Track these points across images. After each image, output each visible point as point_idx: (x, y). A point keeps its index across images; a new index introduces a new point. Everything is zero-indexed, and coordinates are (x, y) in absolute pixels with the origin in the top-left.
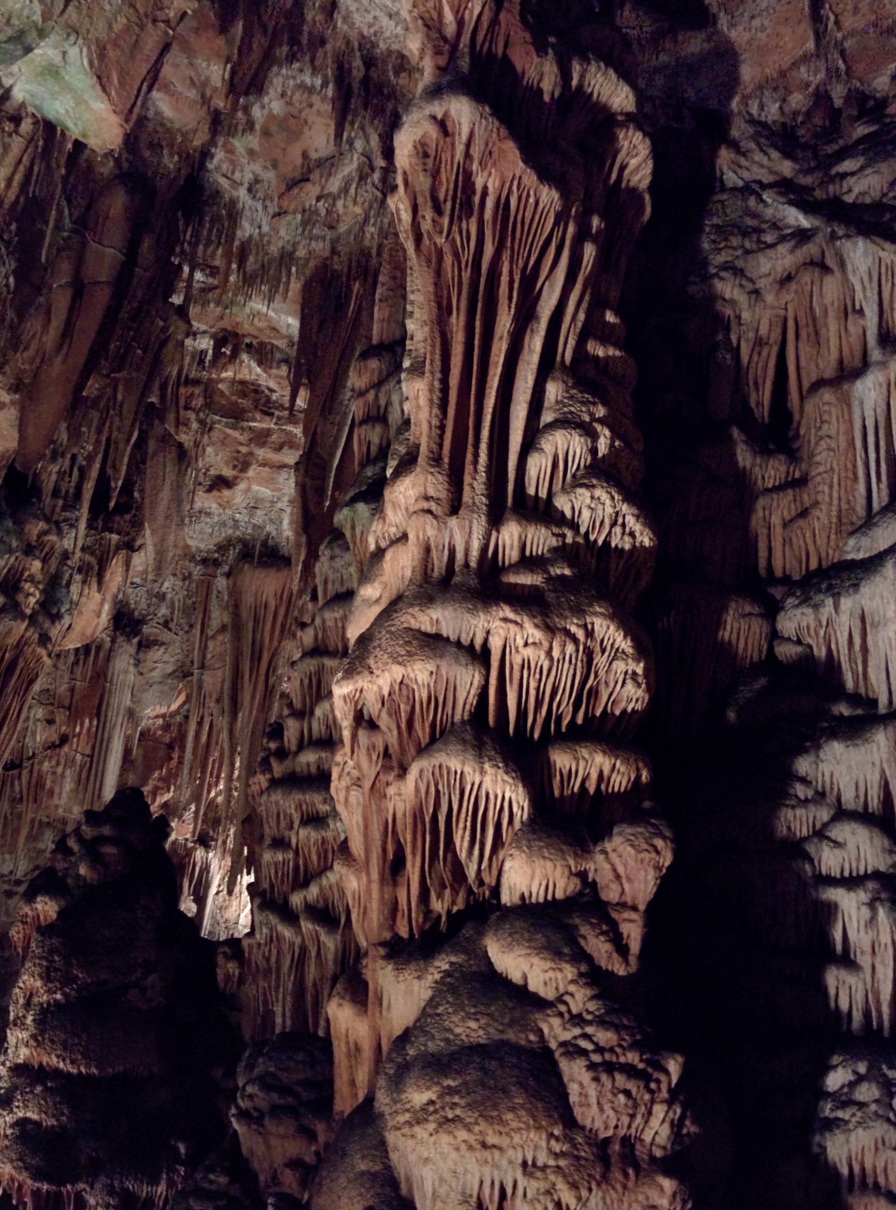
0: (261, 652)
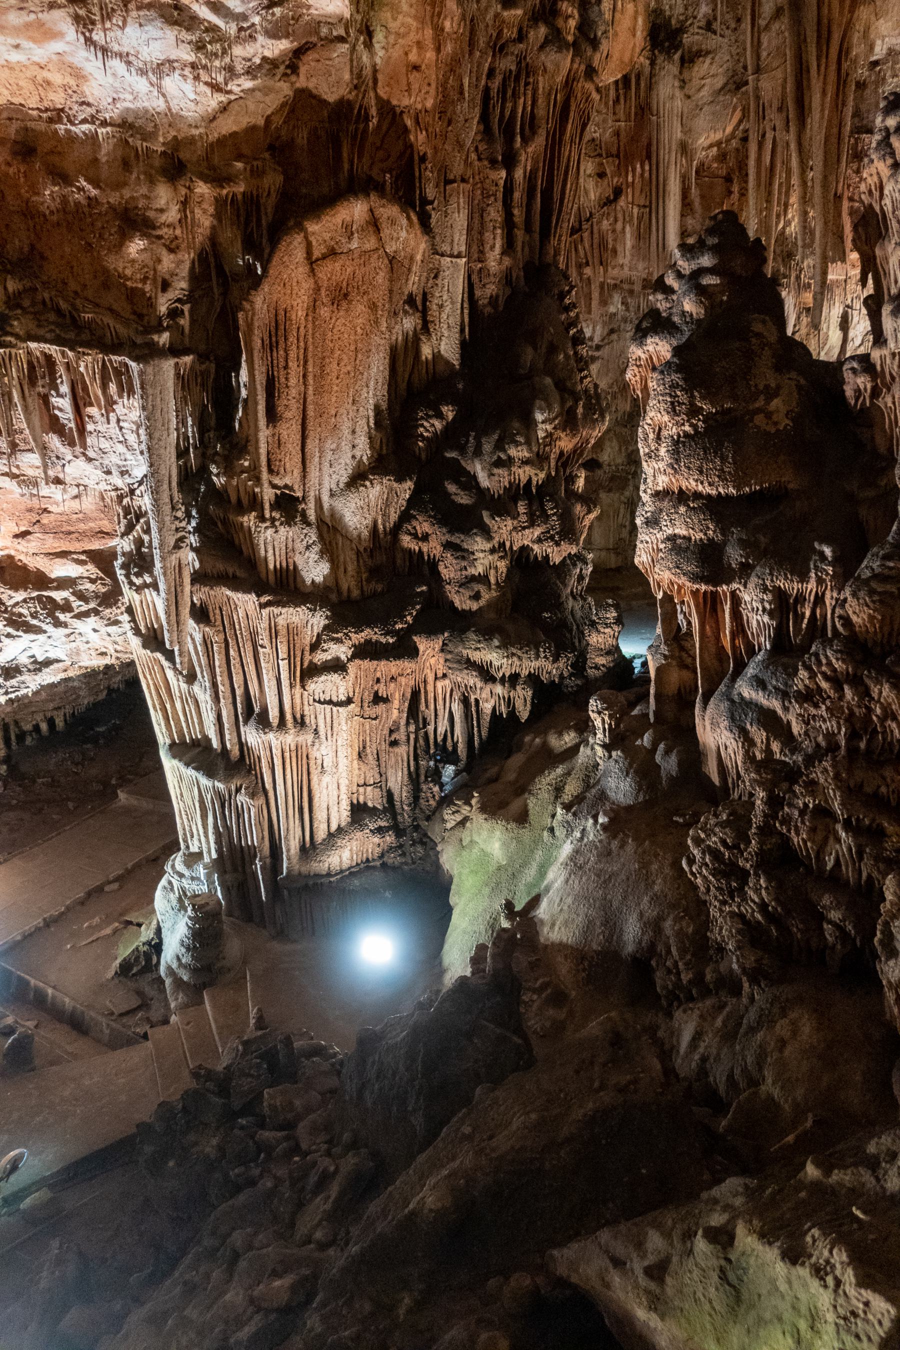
0: (829, 32)
